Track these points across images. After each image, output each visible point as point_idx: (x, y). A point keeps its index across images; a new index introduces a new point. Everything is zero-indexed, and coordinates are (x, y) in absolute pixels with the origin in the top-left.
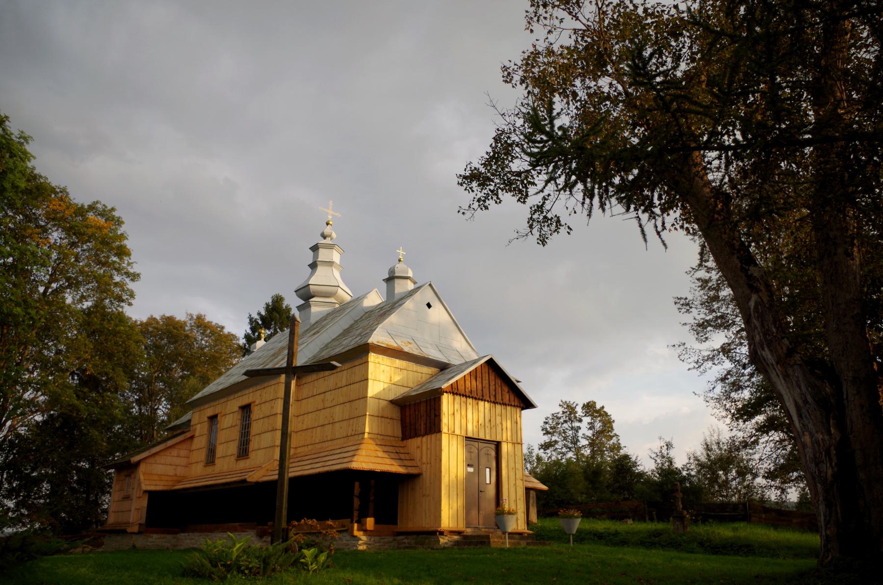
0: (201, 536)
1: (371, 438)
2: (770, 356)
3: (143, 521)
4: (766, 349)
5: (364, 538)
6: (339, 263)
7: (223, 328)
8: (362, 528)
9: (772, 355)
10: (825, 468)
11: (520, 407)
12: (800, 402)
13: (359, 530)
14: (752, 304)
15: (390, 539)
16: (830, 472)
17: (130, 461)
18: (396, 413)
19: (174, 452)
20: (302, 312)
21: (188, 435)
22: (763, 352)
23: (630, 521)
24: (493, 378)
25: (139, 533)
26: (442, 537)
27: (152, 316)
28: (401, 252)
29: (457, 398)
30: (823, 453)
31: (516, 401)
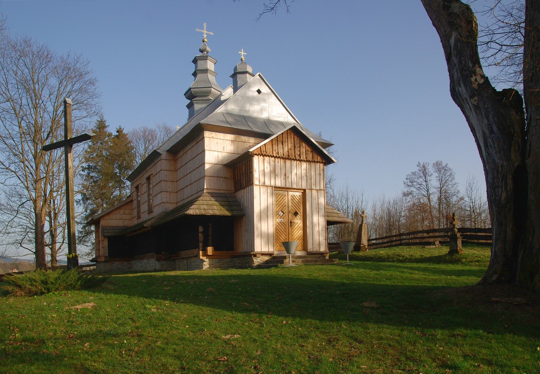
1: (209, 193)
2: (464, 91)
3: (107, 255)
4: (462, 85)
5: (207, 260)
6: (213, 71)
8: (205, 254)
9: (466, 90)
10: (500, 192)
11: (322, 162)
12: (487, 132)
13: (203, 256)
14: (452, 41)
16: (504, 195)
19: (122, 211)
22: (460, 88)
23: (151, 262)
24: (298, 142)
25: (105, 261)
26: (255, 258)
28: (243, 53)
29: (267, 158)
30: (501, 178)
31: (319, 158)
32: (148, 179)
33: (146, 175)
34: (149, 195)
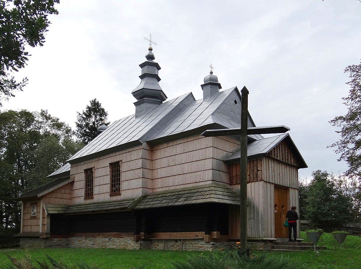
0: (87, 239)
7: (58, 119)
15: (226, 243)
17: (37, 196)
18: (223, 167)
20: (138, 106)
21: (70, 181)
27: (95, 100)
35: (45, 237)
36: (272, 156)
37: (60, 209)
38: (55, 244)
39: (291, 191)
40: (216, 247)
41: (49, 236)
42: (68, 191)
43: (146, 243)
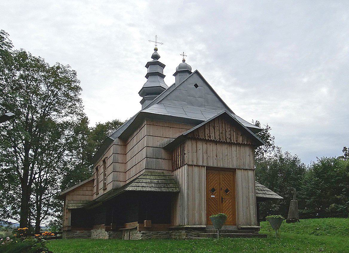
18: (163, 154)
32: (104, 162)
33: (103, 159)
34: (105, 175)
35: (66, 229)
36: (200, 137)
37: (80, 205)
38: (77, 236)
39: (239, 173)
40: (147, 236)
41: (70, 228)
42: (89, 189)
43: (116, 233)
